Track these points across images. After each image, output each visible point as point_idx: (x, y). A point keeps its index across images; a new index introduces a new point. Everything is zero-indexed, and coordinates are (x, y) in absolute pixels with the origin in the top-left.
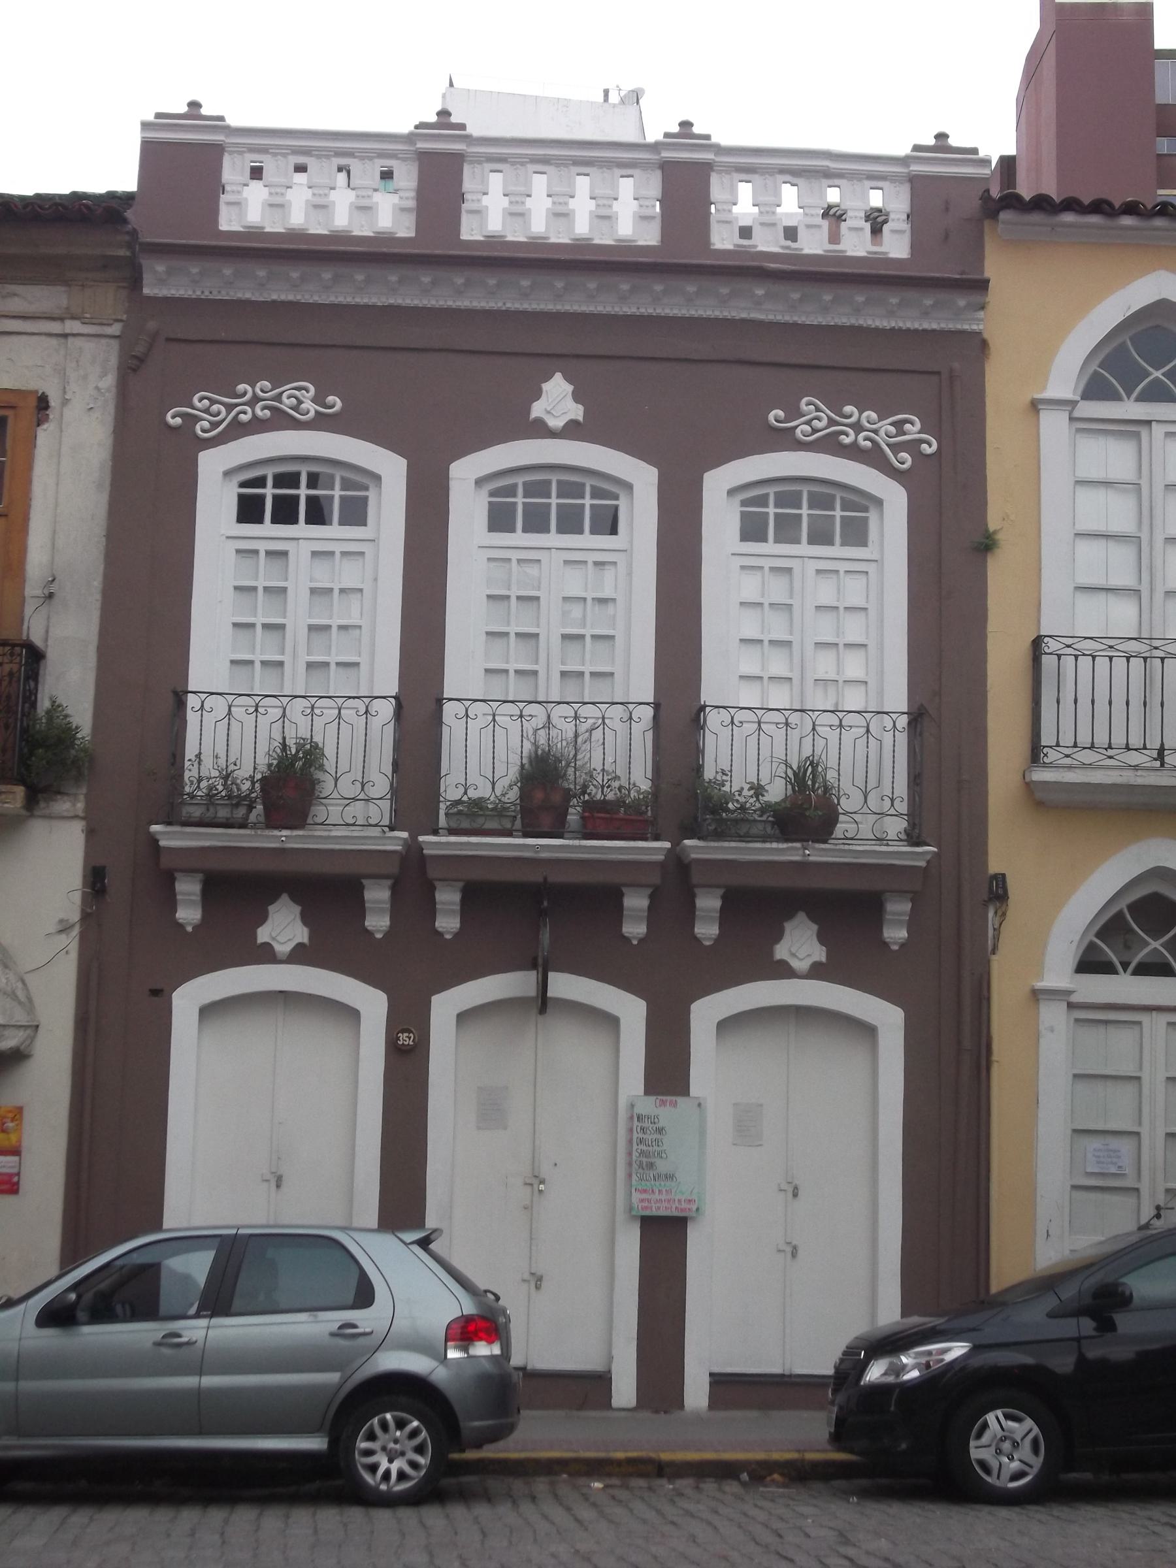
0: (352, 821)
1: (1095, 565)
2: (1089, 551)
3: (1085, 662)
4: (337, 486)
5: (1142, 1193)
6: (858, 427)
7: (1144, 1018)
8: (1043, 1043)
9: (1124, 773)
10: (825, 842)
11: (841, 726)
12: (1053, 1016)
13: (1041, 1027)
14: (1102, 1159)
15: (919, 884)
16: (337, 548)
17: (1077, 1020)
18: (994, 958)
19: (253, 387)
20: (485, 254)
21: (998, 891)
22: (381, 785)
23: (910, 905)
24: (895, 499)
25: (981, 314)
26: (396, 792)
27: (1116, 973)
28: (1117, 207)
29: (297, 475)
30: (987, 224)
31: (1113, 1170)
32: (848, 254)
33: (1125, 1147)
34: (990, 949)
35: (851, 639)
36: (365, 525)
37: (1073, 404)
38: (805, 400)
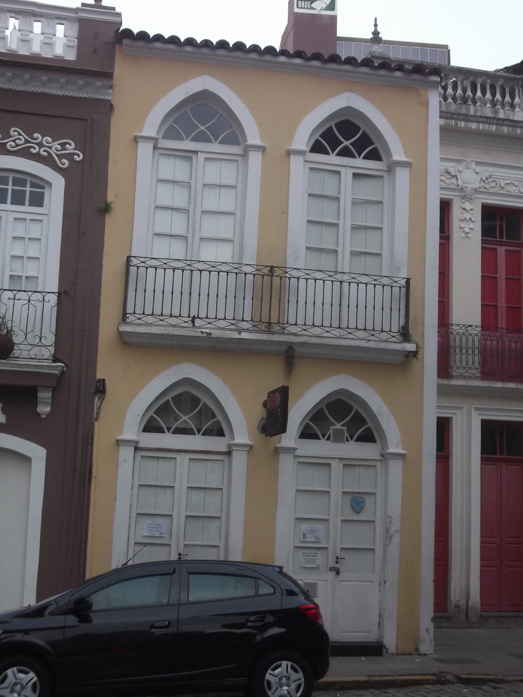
0: (34, 357)
1: (164, 222)
2: (162, 217)
3: (151, 271)
4: (28, 185)
5: (172, 546)
6: (41, 145)
7: (178, 456)
8: (120, 468)
9: (167, 328)
10: (5, 359)
11: (14, 299)
12: (126, 454)
13: (120, 460)
14: (152, 529)
15: (58, 383)
16: (28, 217)
17: (298, 463)
18: (96, 423)
19: (43, 138)
20: (24, 61)
21: (100, 388)
22: (50, 339)
23: (51, 394)
24: (58, 184)
25: (111, 90)
26: (57, 343)
27: (195, 434)
28: (359, 61)
29: (7, 178)
30: (117, 47)
31: (157, 534)
32: (43, 56)
33: (164, 522)
34: (95, 417)
35: (31, 254)
36: (6, 203)
37: (156, 140)
38: (13, 129)
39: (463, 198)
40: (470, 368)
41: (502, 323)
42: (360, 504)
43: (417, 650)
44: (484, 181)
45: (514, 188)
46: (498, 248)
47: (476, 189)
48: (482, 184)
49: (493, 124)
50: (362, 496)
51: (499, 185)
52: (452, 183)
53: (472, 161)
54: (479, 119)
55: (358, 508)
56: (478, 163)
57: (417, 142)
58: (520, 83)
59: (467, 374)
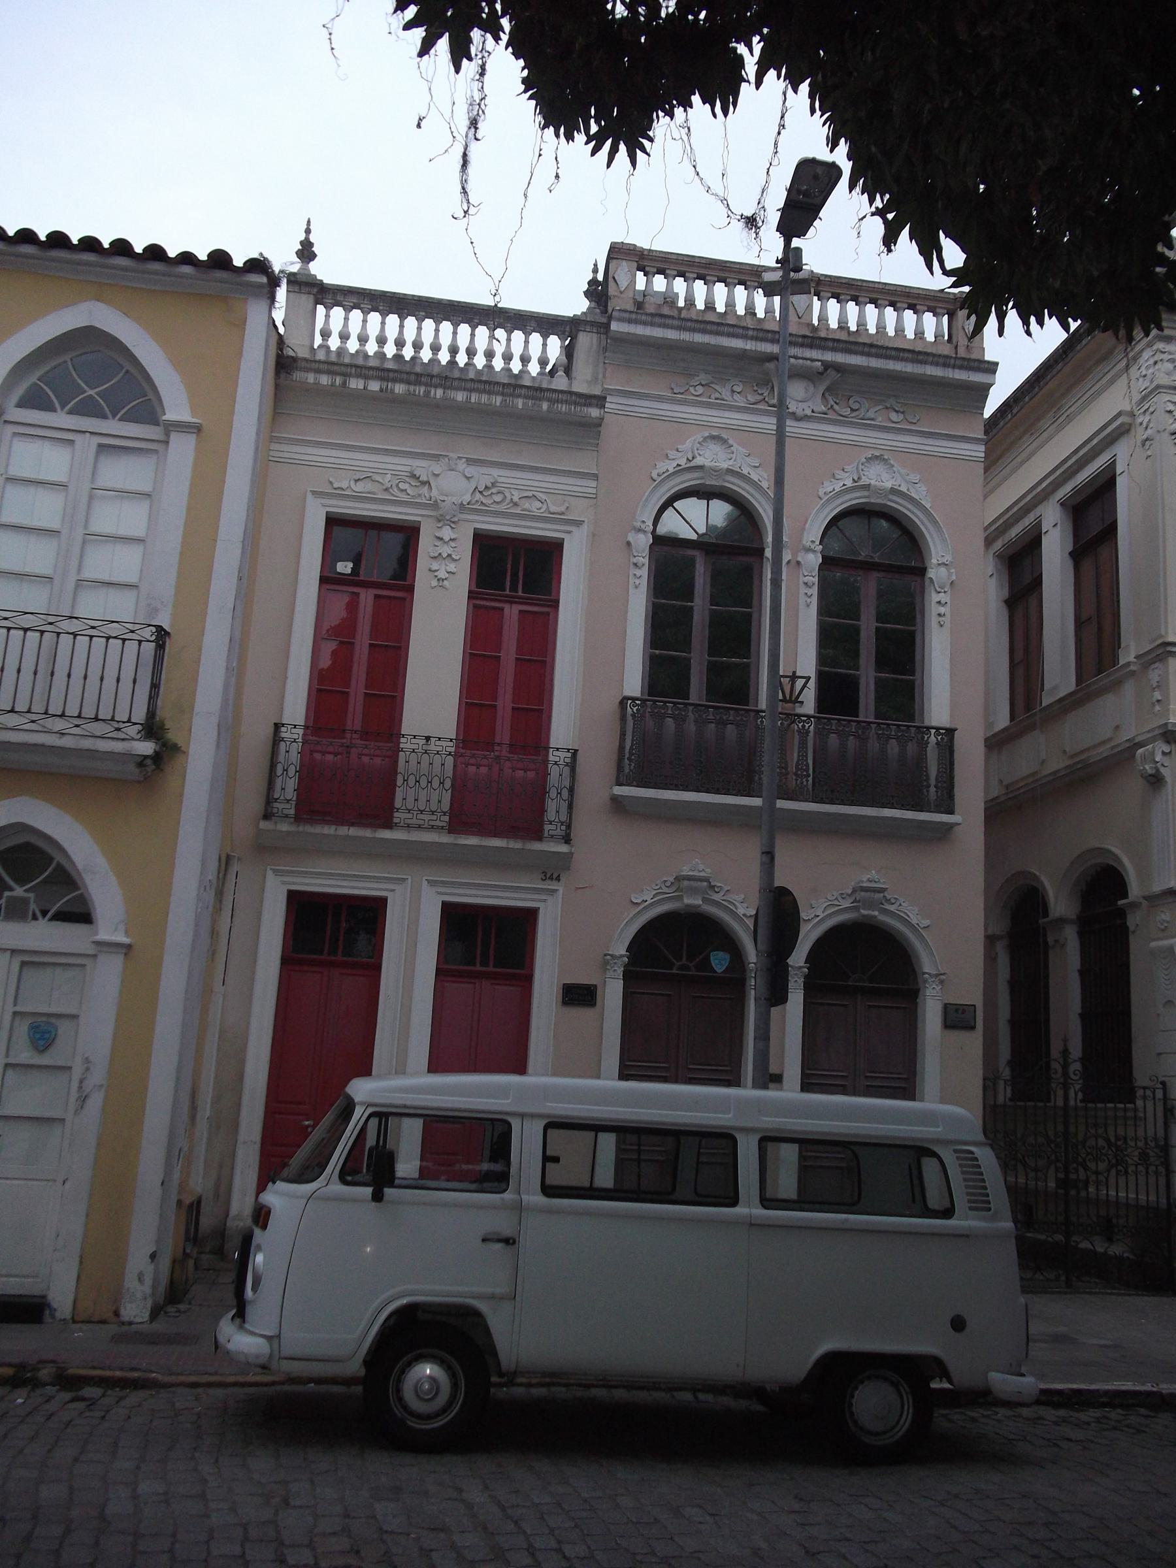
39: (439, 521)
40: (422, 812)
41: (503, 732)
42: (47, 1036)
43: (117, 1314)
44: (481, 492)
45: (539, 504)
46: (507, 607)
47: (462, 503)
48: (478, 496)
49: (497, 394)
50: (53, 1020)
51: (508, 500)
52: (420, 495)
53: (460, 458)
54: (469, 385)
55: (42, 1043)
56: (471, 462)
57: (215, 391)
58: (568, 329)
59: (414, 821)
